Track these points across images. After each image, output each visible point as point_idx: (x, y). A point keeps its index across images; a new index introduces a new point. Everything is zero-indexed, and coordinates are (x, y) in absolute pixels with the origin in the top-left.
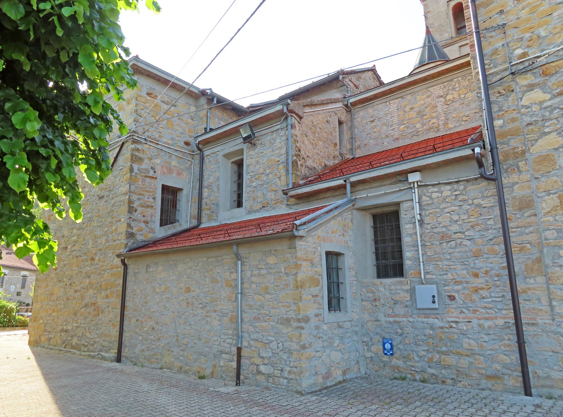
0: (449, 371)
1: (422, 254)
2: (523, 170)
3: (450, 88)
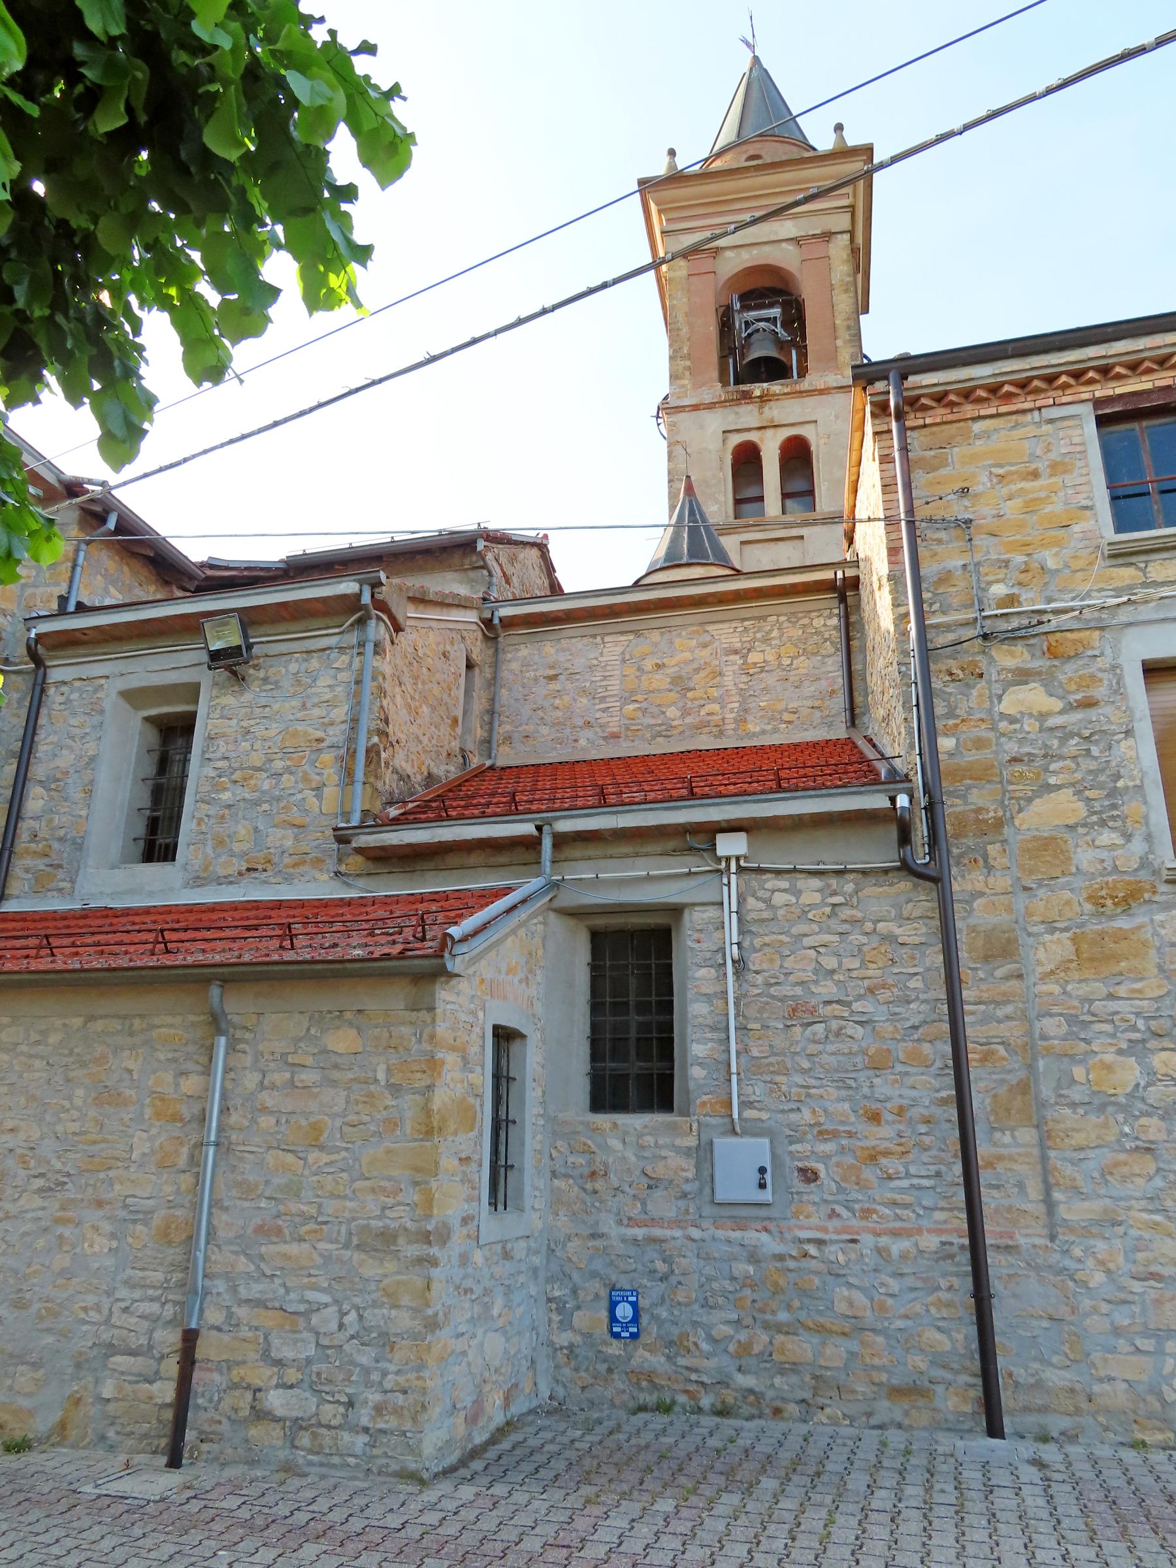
0: (794, 1379)
1: (738, 1053)
2: (996, 864)
3: (759, 635)
